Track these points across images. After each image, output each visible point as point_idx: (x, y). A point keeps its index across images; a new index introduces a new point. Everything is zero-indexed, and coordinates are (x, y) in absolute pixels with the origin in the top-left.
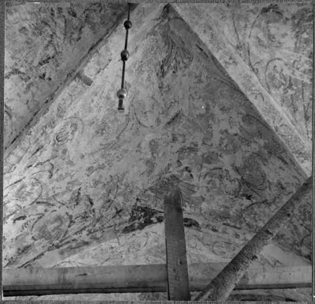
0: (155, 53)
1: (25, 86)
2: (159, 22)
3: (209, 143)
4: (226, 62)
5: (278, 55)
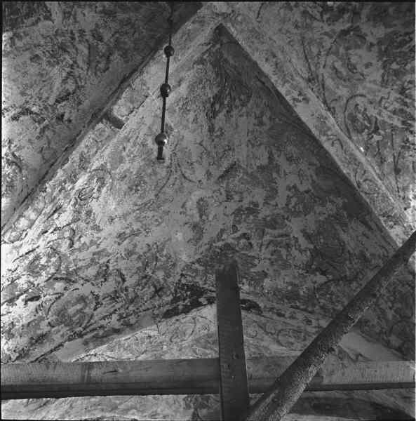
0: (204, 87)
1: (38, 130)
2: (209, 46)
3: (273, 203)
4: (294, 99)
5: (360, 90)
